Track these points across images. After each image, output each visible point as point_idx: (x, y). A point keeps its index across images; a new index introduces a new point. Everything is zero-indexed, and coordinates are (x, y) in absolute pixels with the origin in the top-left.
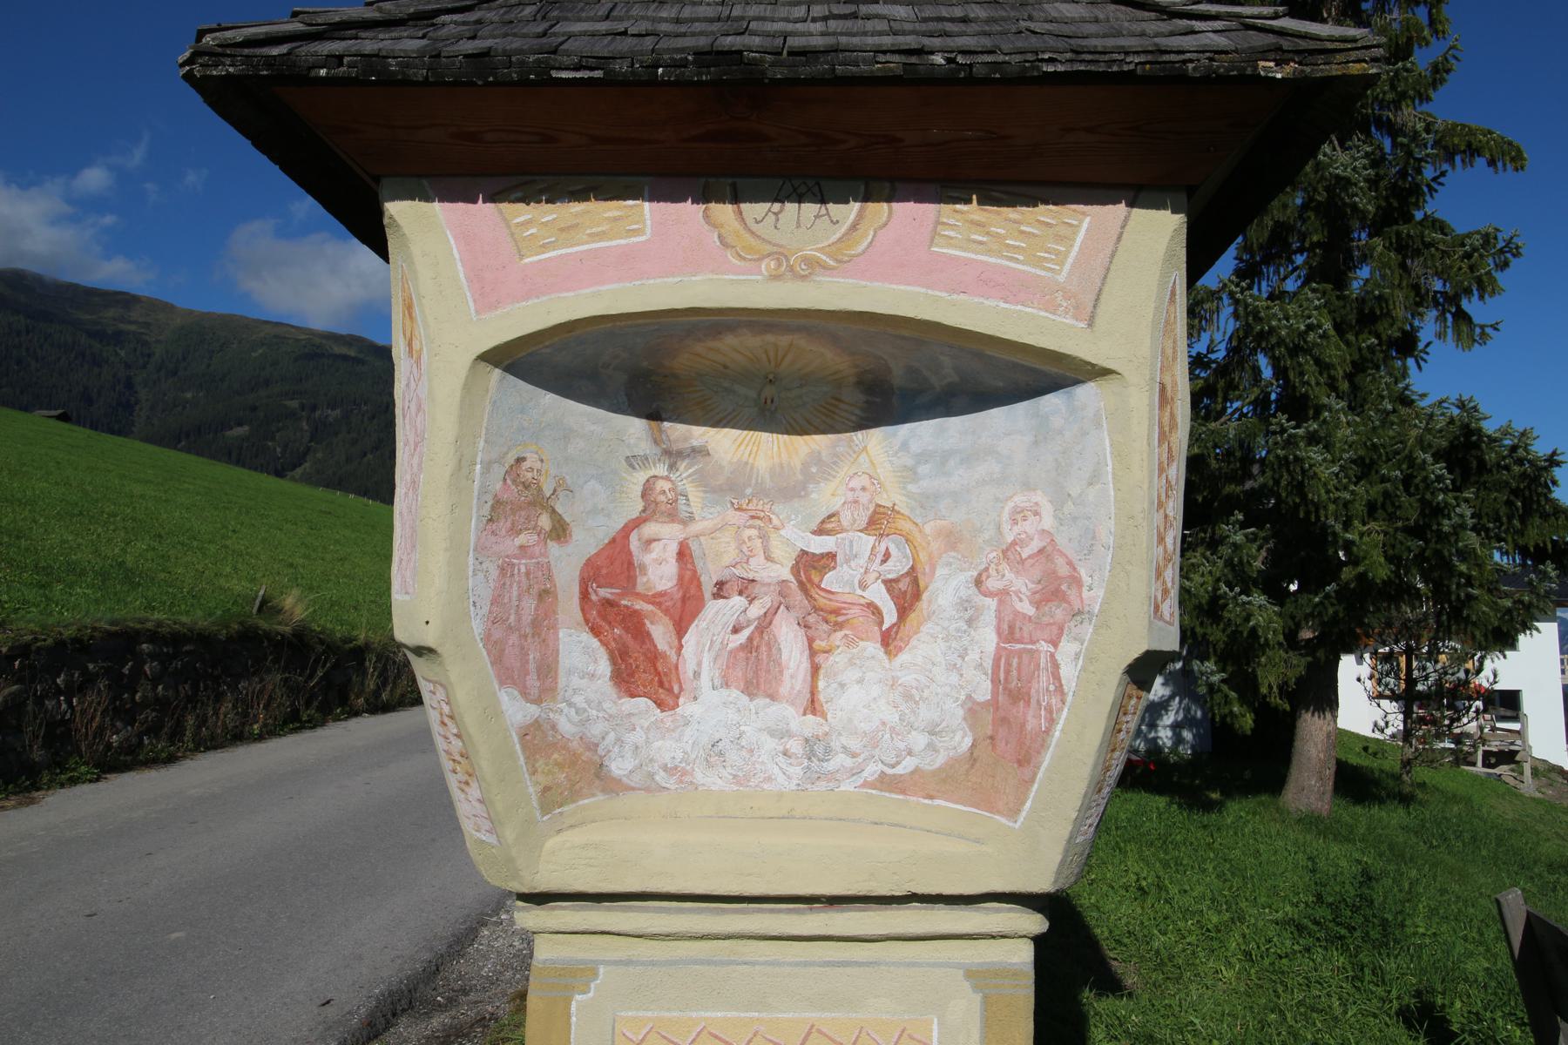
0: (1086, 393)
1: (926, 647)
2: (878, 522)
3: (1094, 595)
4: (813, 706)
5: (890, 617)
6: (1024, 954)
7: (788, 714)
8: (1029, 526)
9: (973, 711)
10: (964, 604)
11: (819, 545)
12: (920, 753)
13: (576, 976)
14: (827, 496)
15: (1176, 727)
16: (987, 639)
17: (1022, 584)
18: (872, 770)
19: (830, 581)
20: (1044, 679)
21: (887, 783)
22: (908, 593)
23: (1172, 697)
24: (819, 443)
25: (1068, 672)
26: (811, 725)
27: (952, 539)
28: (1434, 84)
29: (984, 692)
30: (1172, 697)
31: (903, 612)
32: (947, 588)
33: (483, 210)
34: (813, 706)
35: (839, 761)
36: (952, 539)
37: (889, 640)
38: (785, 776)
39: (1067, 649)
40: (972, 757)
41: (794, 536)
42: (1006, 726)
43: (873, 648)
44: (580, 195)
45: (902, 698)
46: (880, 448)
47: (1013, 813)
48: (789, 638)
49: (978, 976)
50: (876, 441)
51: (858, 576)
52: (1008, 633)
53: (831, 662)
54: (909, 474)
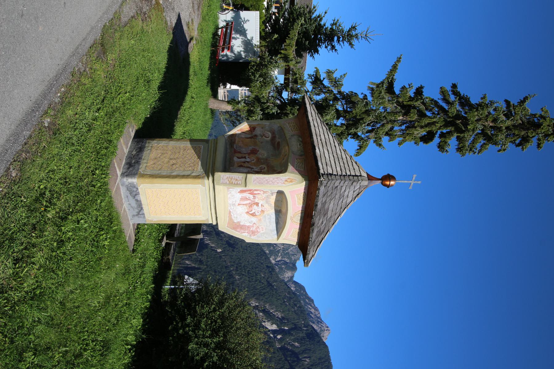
0: (276, 236)
1: (247, 217)
2: (263, 211)
3: (253, 237)
4: (239, 204)
5: (250, 213)
6: (210, 222)
7: (238, 202)
8: (261, 229)
9: (239, 222)
10: (252, 221)
11: (260, 205)
12: (234, 216)
13: (204, 185)
14: (266, 206)
15: (226, 55)
16: (248, 224)
17: (254, 229)
18: (231, 210)
19: (255, 206)
20: (243, 231)
21: (230, 212)
22: (253, 215)
23: (234, 54)
24: (273, 205)
25: (244, 234)
26: (237, 204)
27: (260, 220)
28: (377, 144)
29: (241, 224)
30: (234, 54)
31: (251, 214)
32: (254, 219)
33: (303, 191)
34: (239, 204)
35: (232, 207)
36: (260, 220)
37: (248, 212)
38: (230, 202)
39: (247, 234)
40: (234, 222)
41: (261, 203)
42: (238, 226)
43: (247, 211)
44: (304, 200)
45: (240, 215)
46: (273, 212)
47: (228, 227)
48: (248, 202)
49: (208, 220)
50: (273, 211)
51: (255, 209)
52: (249, 227)
53: (245, 207)
54: (268, 215)
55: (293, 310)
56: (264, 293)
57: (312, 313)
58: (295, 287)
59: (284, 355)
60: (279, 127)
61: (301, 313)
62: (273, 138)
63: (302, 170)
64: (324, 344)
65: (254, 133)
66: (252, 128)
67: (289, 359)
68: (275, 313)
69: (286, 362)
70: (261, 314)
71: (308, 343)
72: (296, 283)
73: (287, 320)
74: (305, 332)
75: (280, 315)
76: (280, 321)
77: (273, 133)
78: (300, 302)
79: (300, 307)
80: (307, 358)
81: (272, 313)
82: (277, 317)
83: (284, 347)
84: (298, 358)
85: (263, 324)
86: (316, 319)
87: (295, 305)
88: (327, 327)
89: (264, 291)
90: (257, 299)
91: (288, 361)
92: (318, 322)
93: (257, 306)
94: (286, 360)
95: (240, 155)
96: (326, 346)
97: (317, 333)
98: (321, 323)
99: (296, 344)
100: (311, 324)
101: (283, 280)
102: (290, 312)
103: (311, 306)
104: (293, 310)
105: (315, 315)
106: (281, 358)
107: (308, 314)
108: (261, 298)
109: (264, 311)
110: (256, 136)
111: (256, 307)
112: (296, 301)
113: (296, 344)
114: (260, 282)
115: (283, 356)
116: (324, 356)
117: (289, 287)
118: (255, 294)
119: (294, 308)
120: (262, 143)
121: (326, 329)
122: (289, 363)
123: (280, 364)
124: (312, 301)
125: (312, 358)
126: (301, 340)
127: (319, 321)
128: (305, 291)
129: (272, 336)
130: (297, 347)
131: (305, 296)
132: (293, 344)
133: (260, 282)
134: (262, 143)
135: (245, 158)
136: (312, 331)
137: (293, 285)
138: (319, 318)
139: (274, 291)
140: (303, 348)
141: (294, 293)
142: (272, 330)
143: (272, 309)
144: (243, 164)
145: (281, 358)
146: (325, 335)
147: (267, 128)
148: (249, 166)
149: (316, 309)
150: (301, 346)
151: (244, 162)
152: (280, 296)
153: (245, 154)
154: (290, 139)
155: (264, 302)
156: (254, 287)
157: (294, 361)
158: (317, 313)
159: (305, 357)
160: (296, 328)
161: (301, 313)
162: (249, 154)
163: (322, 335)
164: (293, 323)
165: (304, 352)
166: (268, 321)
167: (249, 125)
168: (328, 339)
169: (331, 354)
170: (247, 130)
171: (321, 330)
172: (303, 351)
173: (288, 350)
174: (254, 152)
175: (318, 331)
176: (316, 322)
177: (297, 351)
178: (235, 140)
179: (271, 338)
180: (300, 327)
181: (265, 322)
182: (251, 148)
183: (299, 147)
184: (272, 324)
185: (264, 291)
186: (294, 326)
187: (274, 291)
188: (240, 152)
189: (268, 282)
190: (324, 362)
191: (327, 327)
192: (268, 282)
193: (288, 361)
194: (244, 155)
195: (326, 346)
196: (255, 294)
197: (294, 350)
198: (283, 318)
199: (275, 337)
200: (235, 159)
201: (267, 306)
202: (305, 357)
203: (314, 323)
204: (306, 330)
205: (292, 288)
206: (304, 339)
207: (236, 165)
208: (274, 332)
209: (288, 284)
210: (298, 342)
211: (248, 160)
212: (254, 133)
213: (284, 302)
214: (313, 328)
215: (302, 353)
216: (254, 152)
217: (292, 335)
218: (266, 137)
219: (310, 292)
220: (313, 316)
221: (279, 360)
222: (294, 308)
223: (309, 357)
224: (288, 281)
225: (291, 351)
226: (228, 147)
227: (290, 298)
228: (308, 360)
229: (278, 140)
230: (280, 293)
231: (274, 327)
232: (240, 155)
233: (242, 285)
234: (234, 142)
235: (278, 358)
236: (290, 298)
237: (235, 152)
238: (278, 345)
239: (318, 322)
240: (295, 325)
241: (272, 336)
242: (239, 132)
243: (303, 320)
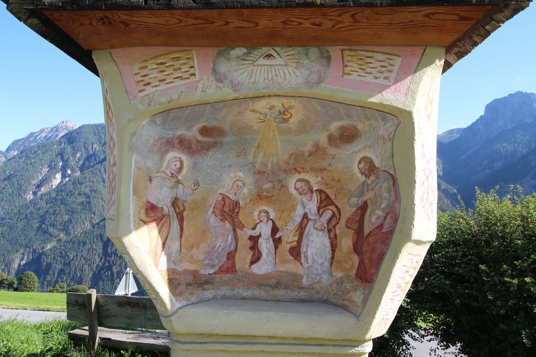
55: (41, 155)
56: (19, 184)
57: (46, 136)
58: (14, 150)
59: (88, 168)
60: (153, 122)
61: (45, 147)
62: (184, 144)
63: (398, 61)
64: (80, 128)
65: (167, 209)
66: (152, 212)
67: (92, 164)
68: (44, 174)
69: (95, 166)
70: (43, 189)
71: (78, 144)
72: (9, 149)
73: (52, 162)
74: (66, 146)
75: (45, 170)
76: (52, 168)
77: (169, 144)
78: (32, 147)
79: (38, 148)
80: (93, 146)
81: (43, 178)
82: (48, 172)
83: (80, 167)
84: (92, 155)
85: (54, 187)
86: (53, 132)
87: (36, 152)
88: (63, 122)
89: (16, 184)
90: (25, 193)
91: (94, 165)
92: (57, 131)
93: (33, 192)
94: (93, 166)
95: (244, 256)
96: (83, 126)
97: (68, 133)
98: (58, 128)
99: (78, 155)
100: (58, 138)
101: (4, 162)
102: (43, 158)
103: (38, 136)
104: (41, 155)
105: (49, 132)
106: (91, 171)
107: (47, 140)
108: (23, 188)
109: (39, 186)
110: (175, 203)
111: (35, 193)
112: (31, 151)
113: (78, 155)
114: (4, 188)
115: (89, 170)
116: (92, 130)
117: (13, 157)
118: (19, 195)
119: (39, 154)
120: (197, 184)
121: (65, 124)
122: (97, 164)
123: (96, 173)
124: (32, 134)
125: (94, 141)
126: (74, 150)
127: (56, 129)
128: (20, 140)
129: (67, 179)
130: (81, 155)
131: (25, 141)
132: (78, 159)
133: (4, 188)
134: (197, 184)
135: (255, 240)
136: (66, 139)
137: (12, 153)
138: (52, 129)
139: (17, 173)
140: (83, 149)
141: (22, 152)
142: (62, 179)
143: (38, 177)
144: (285, 247)
145: (91, 171)
146: (71, 126)
147: (150, 163)
148: (292, 226)
149: (42, 131)
150: (81, 151)
151: (277, 242)
152: (23, 168)
153: (236, 239)
154: (235, 87)
155: (29, 185)
156: (10, 195)
157: (95, 159)
158: (47, 131)
159: (92, 148)
160: (61, 154)
161: (45, 147)
162: (237, 226)
163: (71, 129)
164: (56, 157)
165: (86, 149)
166: (51, 182)
167: (137, 227)
168: (75, 123)
169: (91, 123)
170: (156, 231)
171: (66, 128)
172: (86, 149)
173: (83, 164)
174: (230, 211)
175: (67, 132)
176: (57, 133)
177: (85, 156)
178: (186, 272)
179: (70, 181)
180: (61, 150)
181: (52, 186)
182: (213, 221)
183: (278, 61)
184: (55, 178)
185: (16, 184)
186: (60, 156)
187: (17, 173)
188: (231, 256)
189: (5, 179)
190: (98, 130)
191: (63, 122)
192: (5, 179)
193: (94, 165)
194: (244, 243)
195: (83, 127)
196: (19, 195)
197: (84, 158)
198: (49, 166)
199: (69, 176)
200: (261, 269)
201: (35, 182)
202: (92, 148)
203: (57, 135)
204: (65, 144)
205: (15, 154)
206: (73, 147)
207: (292, 267)
208: (64, 176)
209: (9, 158)
210: (76, 154)
211: (265, 229)
212: (167, 209)
213: (31, 164)
214: (62, 137)
215: (88, 151)
216: (230, 211)
217: (68, 159)
218: (181, 169)
219: (23, 134)
220: (50, 135)
221: (93, 173)
222: (39, 154)
223: (92, 144)
224: (6, 157)
225: (85, 162)
226: (209, 294)
227: (27, 157)
228: (95, 146)
229: (192, 133)
230: (19, 167)
231: (59, 176)
232: (244, 256)
233: (6, 209)
234: (195, 273)
235: (91, 174)
236: (27, 157)
237: (229, 267)
238: (78, 174)
239: (57, 131)
240: (58, 155)
241: (67, 179)
242: (163, 259)
243: (53, 145)
